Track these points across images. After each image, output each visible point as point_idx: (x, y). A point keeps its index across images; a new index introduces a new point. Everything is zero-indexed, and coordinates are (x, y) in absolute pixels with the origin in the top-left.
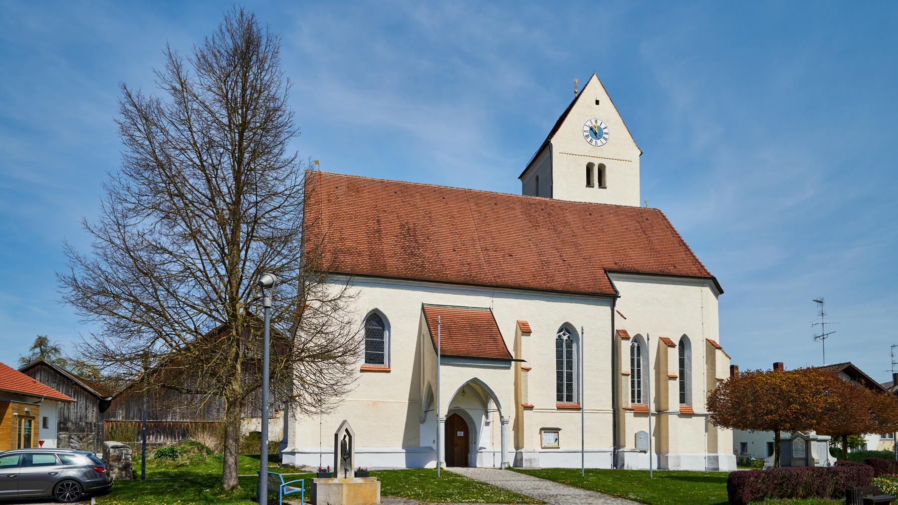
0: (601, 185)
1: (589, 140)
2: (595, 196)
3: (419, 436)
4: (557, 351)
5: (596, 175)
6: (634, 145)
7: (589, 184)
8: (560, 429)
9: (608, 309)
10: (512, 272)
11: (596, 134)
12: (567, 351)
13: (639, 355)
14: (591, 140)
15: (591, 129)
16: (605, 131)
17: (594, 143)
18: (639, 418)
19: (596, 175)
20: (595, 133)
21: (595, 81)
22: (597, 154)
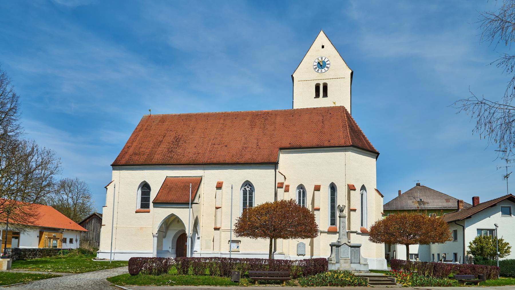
0: (325, 95)
1: (316, 70)
2: (322, 103)
3: (162, 245)
4: (244, 197)
5: (322, 90)
6: (347, 67)
7: (317, 95)
8: (359, 247)
9: (274, 170)
10: (222, 155)
11: (321, 66)
12: (250, 197)
13: (304, 197)
14: (318, 70)
15: (319, 63)
16: (327, 63)
17: (320, 72)
18: (458, 238)
19: (322, 90)
20: (321, 65)
21: (322, 35)
22: (321, 78)
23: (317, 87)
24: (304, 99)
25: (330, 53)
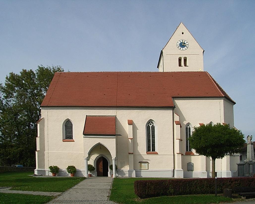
1: (179, 48)
2: (183, 69)
5: (182, 61)
7: (180, 65)
20: (182, 45)
22: (183, 53)
23: (180, 60)
24: (170, 65)
25: (188, 38)
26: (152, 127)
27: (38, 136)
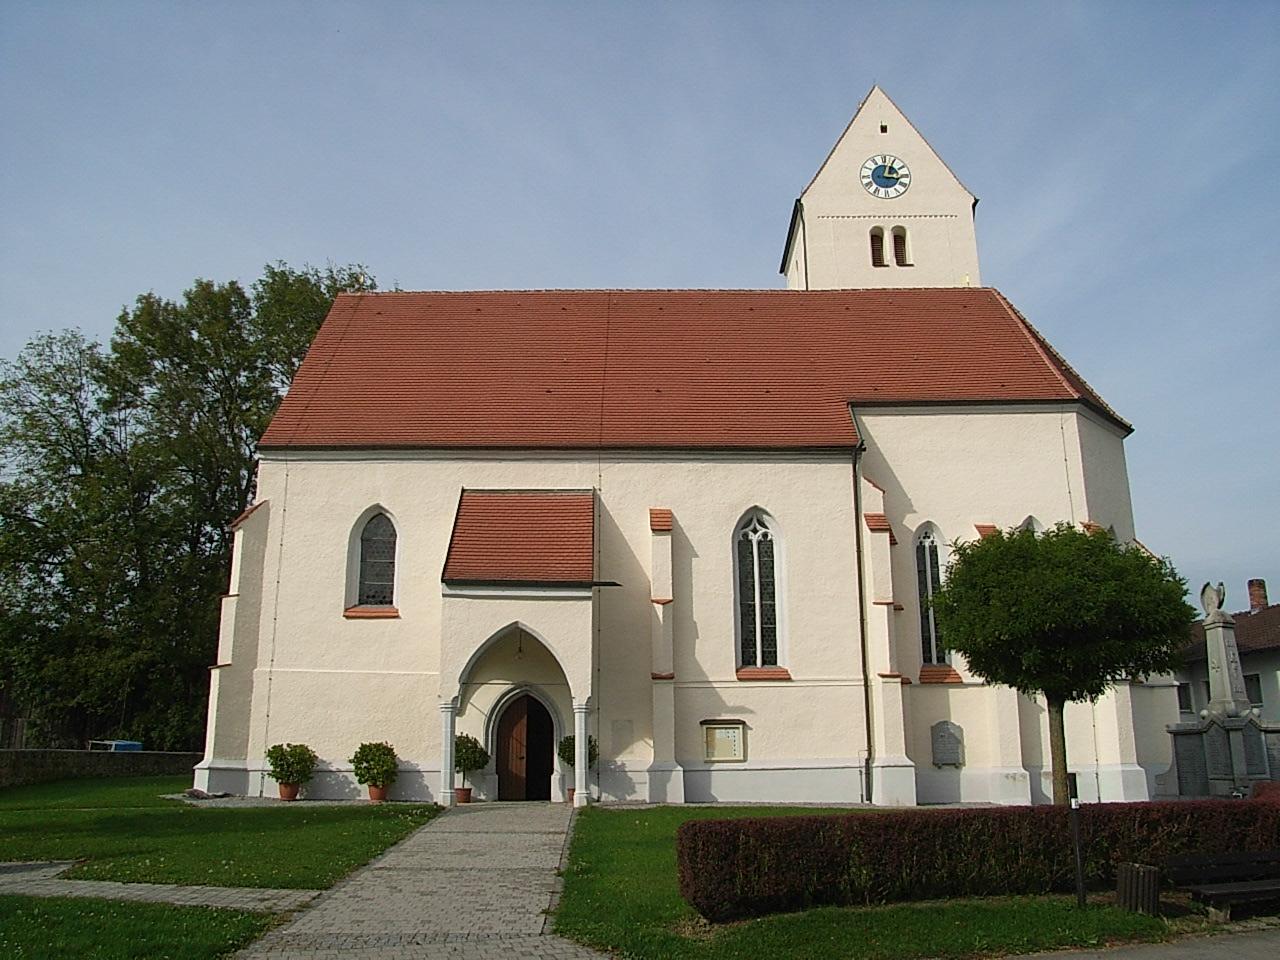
1: (872, 189)
2: (892, 278)
7: (878, 261)
17: (905, 180)
22: (887, 210)
23: (876, 238)
24: (833, 263)
25: (905, 146)
26: (759, 543)
27: (231, 593)
